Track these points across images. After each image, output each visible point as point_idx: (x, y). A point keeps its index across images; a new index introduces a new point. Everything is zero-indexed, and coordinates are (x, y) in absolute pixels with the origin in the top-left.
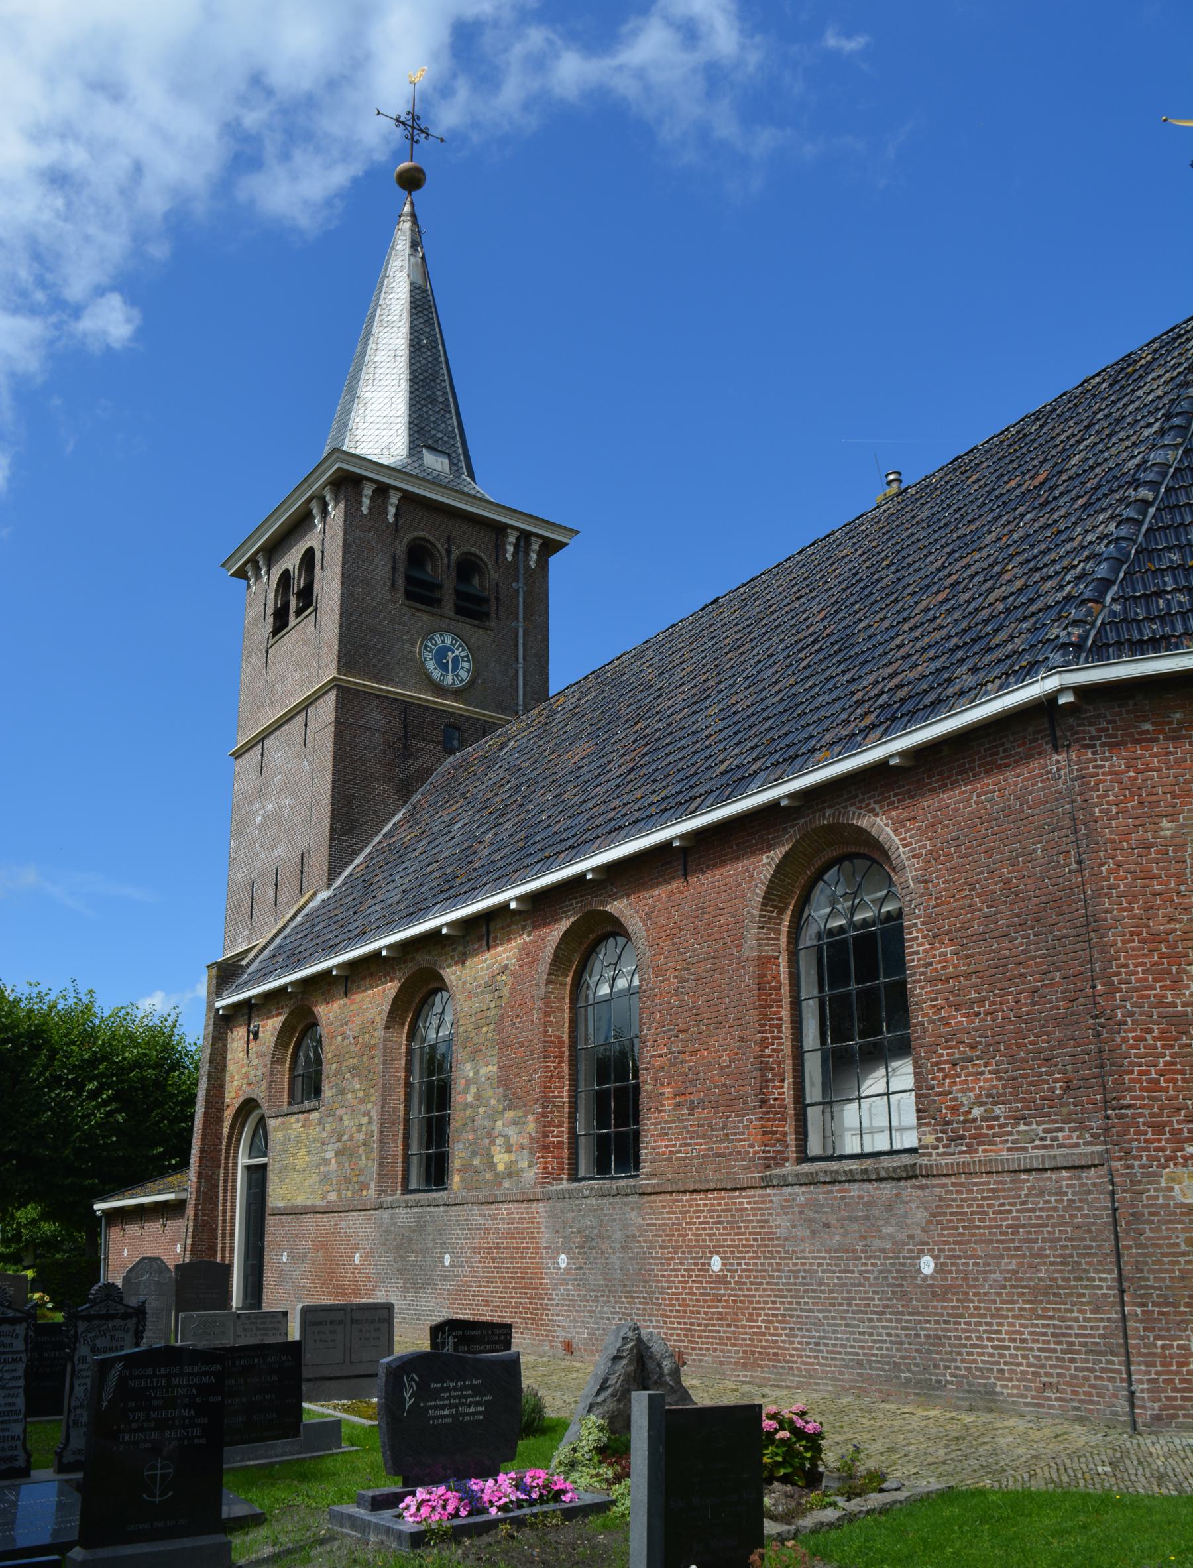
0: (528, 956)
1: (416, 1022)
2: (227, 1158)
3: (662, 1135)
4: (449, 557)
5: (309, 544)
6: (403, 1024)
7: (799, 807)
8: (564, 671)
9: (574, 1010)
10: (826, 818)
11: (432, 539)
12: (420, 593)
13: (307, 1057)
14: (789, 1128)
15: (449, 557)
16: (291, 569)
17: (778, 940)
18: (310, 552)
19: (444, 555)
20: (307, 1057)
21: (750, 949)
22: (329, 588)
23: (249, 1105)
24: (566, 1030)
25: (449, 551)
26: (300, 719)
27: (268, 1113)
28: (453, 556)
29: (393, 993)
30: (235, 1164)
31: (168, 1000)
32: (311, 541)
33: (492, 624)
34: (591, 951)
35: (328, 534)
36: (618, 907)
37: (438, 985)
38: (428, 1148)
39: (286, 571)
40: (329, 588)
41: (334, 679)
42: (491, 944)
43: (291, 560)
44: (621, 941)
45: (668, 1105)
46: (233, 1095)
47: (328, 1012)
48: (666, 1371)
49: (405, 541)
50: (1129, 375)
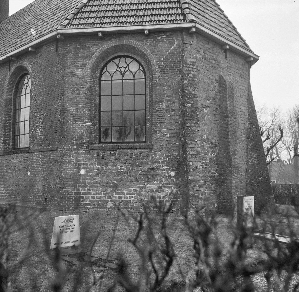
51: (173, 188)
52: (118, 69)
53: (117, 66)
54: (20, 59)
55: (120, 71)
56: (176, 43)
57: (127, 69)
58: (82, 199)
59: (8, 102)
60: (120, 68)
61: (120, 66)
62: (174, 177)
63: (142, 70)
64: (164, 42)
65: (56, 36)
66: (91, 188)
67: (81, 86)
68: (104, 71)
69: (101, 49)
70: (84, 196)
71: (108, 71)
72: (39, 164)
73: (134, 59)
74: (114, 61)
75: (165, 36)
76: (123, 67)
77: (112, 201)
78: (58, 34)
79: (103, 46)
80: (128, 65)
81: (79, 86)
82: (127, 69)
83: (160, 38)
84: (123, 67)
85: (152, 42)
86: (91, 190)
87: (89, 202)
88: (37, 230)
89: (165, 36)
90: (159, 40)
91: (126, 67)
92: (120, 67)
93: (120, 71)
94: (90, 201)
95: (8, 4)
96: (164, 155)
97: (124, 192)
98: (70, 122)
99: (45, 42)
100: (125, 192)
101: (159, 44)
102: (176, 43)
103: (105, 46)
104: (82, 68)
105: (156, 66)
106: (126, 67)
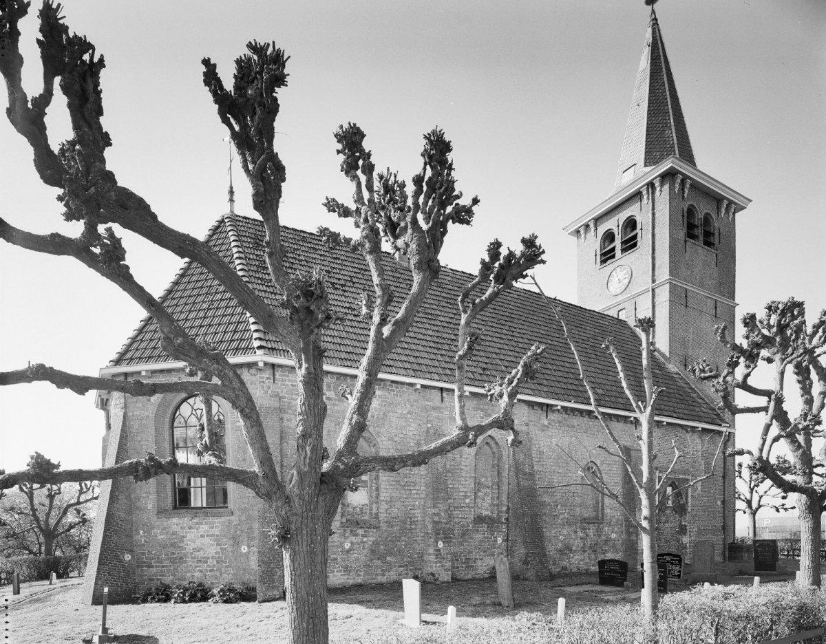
53: (192, 407)
61: (195, 407)
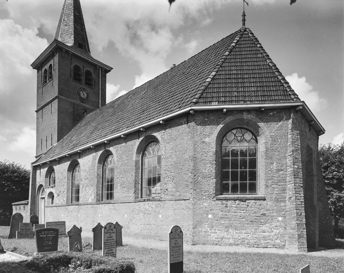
0: (94, 159)
1: (74, 170)
2: (37, 196)
3: (117, 192)
4: (83, 70)
5: (51, 63)
6: (101, 164)
7: (143, 131)
8: (109, 99)
9: (72, 177)
10: (149, 133)
11: (80, 66)
12: (77, 77)
13: (53, 177)
14: (140, 192)
15: (83, 70)
16: (47, 68)
17: (139, 157)
18: (51, 65)
19: (82, 70)
20: (53, 177)
21: (134, 159)
22: (56, 74)
23: (41, 186)
24: (102, 173)
25: (84, 69)
26: (50, 105)
27: (45, 188)
28: (84, 71)
29: (69, 164)
30: (39, 197)
31: (26, 165)
32: (51, 62)
33: (94, 87)
34: (145, 150)
35: (55, 61)
36: (111, 149)
37: (76, 163)
38: (75, 196)
39: (46, 69)
40: (56, 74)
41: (57, 96)
42: (81, 157)
43: (47, 67)
44: (112, 156)
45: (119, 187)
46: (38, 185)
47: (56, 168)
48: (291, 119)
49: (73, 65)
50: (219, 53)
51: (280, 230)
52: (236, 138)
53: (235, 135)
54: (149, 130)
55: (237, 139)
56: (285, 118)
57: (242, 138)
58: (209, 237)
59: (137, 162)
60: (237, 137)
61: (237, 135)
62: (282, 221)
63: (255, 139)
64: (275, 117)
65: (190, 111)
66: (217, 229)
67: (209, 151)
68: (224, 140)
69: (224, 122)
70: (211, 234)
71: (228, 139)
72: (171, 210)
73: (248, 130)
74: (232, 131)
75: (276, 112)
76: (239, 136)
77: (232, 239)
78: (191, 110)
79: (226, 120)
80: (243, 135)
81: (207, 150)
82: (242, 138)
83: (271, 114)
84: (239, 136)
85: (266, 117)
86: (217, 230)
87: (215, 239)
88: (306, 254)
89: (276, 112)
90: (271, 115)
91: (241, 137)
92: (237, 136)
93: (237, 139)
94: (216, 238)
95: (106, 92)
96: (274, 205)
97: (242, 232)
98: (201, 178)
99: (255, 108)
100: (243, 232)
101: (271, 118)
102: (285, 118)
103: (227, 120)
104: (209, 136)
105: (268, 136)
106: (241, 137)
